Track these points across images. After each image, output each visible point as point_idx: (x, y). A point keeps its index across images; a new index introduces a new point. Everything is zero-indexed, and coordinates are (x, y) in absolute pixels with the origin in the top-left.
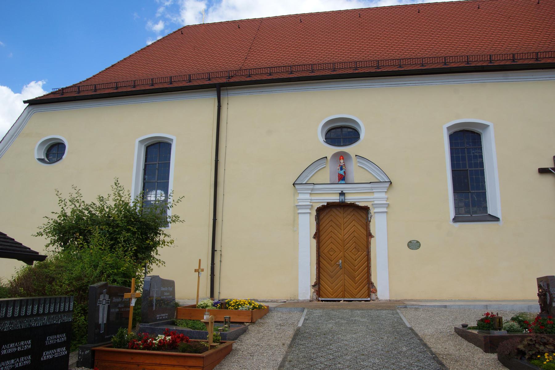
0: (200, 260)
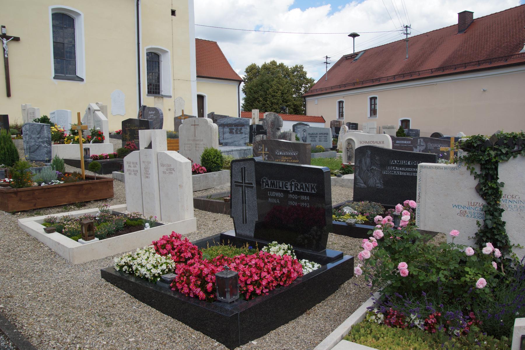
0: (9, 95)
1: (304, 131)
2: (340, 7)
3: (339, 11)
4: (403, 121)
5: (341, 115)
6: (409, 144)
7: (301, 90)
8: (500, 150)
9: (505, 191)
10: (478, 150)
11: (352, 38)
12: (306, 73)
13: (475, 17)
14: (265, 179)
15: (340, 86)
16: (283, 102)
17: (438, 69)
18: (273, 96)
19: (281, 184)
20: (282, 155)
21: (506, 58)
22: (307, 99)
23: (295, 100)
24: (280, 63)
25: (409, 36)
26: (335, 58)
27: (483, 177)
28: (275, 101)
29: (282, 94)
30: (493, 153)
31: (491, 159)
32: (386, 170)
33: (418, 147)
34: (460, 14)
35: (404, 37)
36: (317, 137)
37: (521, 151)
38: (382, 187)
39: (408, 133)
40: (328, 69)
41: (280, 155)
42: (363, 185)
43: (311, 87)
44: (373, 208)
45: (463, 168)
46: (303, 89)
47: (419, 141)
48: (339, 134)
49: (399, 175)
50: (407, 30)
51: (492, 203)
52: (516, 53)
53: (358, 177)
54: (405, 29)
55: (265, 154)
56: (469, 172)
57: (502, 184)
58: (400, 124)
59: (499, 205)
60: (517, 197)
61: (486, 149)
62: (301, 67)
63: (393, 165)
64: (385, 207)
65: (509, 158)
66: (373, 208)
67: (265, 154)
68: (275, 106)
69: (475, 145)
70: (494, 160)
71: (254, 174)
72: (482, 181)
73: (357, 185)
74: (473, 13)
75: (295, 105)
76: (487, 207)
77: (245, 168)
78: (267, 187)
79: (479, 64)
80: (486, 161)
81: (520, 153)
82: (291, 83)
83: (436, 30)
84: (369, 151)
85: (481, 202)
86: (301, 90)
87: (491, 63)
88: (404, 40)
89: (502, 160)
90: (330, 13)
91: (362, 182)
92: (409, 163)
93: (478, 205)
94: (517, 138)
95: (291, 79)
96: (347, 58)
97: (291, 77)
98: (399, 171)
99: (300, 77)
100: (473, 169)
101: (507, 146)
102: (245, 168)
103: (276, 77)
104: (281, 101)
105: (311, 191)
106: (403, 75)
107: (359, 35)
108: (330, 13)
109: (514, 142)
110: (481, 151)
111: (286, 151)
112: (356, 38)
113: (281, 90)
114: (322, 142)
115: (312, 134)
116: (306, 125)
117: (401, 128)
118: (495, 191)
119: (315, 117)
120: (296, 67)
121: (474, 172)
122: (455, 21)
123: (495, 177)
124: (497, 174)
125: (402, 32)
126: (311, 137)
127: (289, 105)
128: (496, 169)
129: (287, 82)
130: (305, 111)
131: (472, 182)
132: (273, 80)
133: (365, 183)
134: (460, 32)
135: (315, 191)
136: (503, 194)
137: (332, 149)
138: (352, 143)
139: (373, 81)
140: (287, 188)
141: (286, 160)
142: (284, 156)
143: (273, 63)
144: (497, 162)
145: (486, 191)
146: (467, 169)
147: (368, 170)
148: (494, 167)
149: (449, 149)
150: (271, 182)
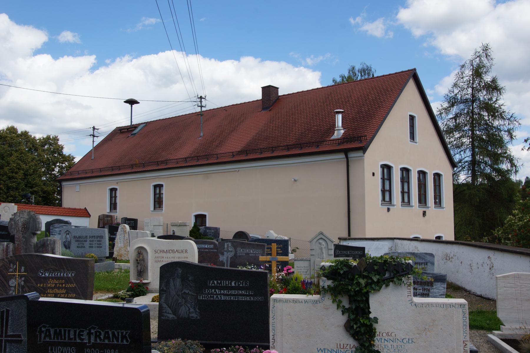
1: (68, 232)
2: (108, 61)
3: (107, 65)
4: (197, 217)
5: (113, 206)
6: (212, 249)
7: (54, 170)
8: (371, 278)
9: (379, 328)
10: (344, 278)
11: (128, 106)
12: (62, 148)
13: (281, 93)
14: (45, 327)
15: (112, 169)
16: (26, 186)
17: (240, 153)
18: (10, 178)
19: (72, 333)
20: (49, 278)
21: (318, 143)
22: (64, 183)
23: (44, 184)
24: (23, 130)
25: (204, 109)
26: (107, 128)
27: (352, 311)
28: (14, 185)
29: (25, 175)
30: (363, 282)
31: (361, 289)
32: (202, 293)
33: (225, 253)
34: (264, 89)
35: (198, 110)
36: (86, 241)
37: (393, 278)
38: (199, 318)
39: (205, 231)
40: (96, 144)
41: (45, 278)
42: (171, 316)
43: (70, 167)
44: (189, 349)
45: (328, 301)
46: (57, 169)
47: (226, 246)
48: (115, 235)
49: (220, 301)
50: (201, 102)
51: (367, 344)
52: (328, 139)
53: (165, 305)
54: (199, 100)
55: (21, 276)
56: (335, 306)
57: (376, 320)
58: (193, 220)
59: (374, 345)
60: (393, 335)
61: (354, 277)
62: (56, 139)
63: (212, 288)
64: (205, 345)
65: (380, 288)
66: (189, 349)
67: (21, 276)
68: (12, 193)
69: (342, 272)
70: (365, 290)
71: (25, 320)
72: (352, 317)
73: (163, 316)
74: (278, 88)
75: (44, 192)
76: (361, 349)
77: (8, 311)
78: (48, 339)
79: (288, 149)
80: (355, 292)
81: (392, 281)
82: (39, 160)
83: (237, 105)
84: (179, 269)
85: (351, 342)
86: (54, 170)
87: (301, 148)
88: (197, 114)
89: (374, 290)
90: (94, 69)
91: (170, 312)
92: (233, 284)
93: (348, 347)
94: (388, 263)
95: (39, 155)
96: (120, 131)
97: (40, 151)
98: (220, 294)
99: (54, 152)
100: (340, 302)
101: (378, 273)
102: (8, 311)
103: (16, 151)
104: (23, 185)
105: (122, 341)
106: (198, 158)
107: (138, 103)
108: (94, 69)
109: (385, 268)
110: (348, 279)
111: (55, 270)
112: (135, 106)
113: (23, 170)
114: (94, 249)
115: (80, 237)
116: (67, 223)
117: (195, 225)
118: (368, 329)
119: (75, 209)
120: (48, 138)
121: (341, 305)
122: (258, 95)
123: (367, 310)
124: (369, 308)
125: (195, 103)
126: (76, 241)
127: (35, 191)
128: (367, 301)
129: (33, 159)
130: (61, 200)
131: (339, 319)
132: (11, 155)
133: (174, 313)
134: (264, 109)
135: (127, 341)
136: (378, 331)
137: (107, 258)
138: (144, 253)
139: (157, 163)
140: (83, 339)
141: (56, 284)
142: (53, 278)
143: (12, 130)
144: (367, 293)
145: (358, 329)
146: (333, 302)
147: (178, 296)
148: (364, 298)
149: (268, 258)
150: (56, 331)
